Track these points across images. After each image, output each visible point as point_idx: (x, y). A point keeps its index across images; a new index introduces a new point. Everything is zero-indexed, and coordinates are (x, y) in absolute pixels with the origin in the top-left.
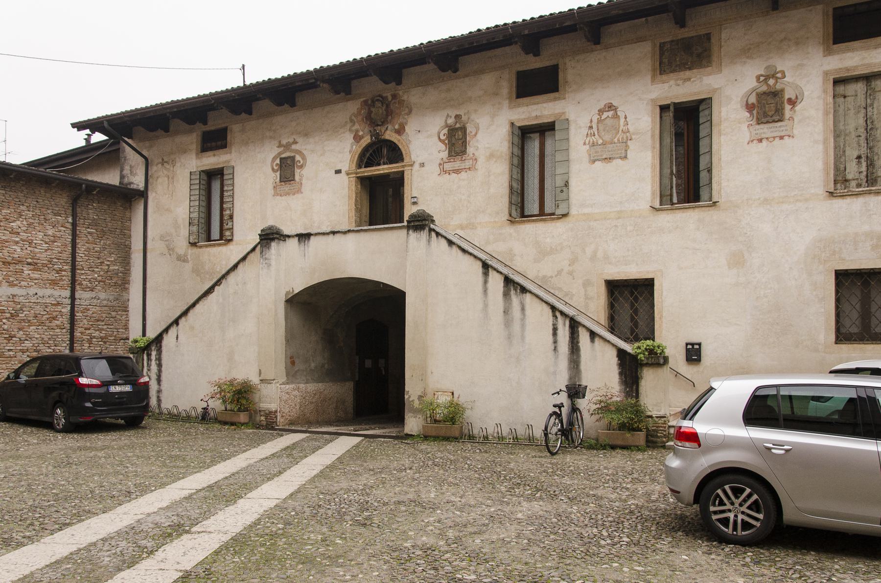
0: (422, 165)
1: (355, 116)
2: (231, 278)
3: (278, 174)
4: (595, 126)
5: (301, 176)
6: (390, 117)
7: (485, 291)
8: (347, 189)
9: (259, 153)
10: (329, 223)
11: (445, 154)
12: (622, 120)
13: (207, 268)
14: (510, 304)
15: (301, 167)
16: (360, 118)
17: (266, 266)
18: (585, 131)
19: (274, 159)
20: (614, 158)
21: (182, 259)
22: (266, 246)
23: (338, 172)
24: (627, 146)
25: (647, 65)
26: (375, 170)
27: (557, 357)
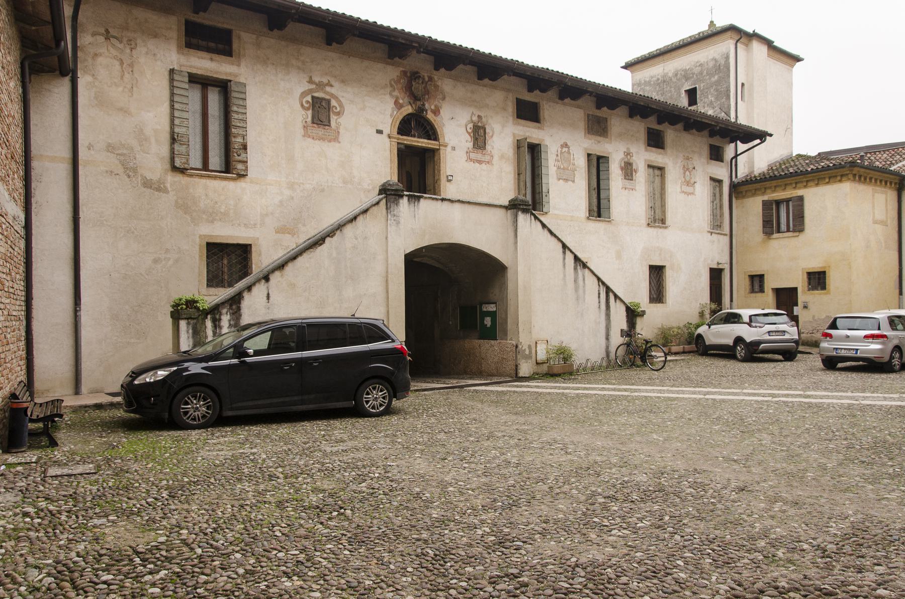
0: (454, 148)
1: (395, 82)
2: (348, 230)
3: (310, 113)
4: (559, 155)
5: (338, 124)
6: (427, 96)
7: (564, 265)
8: (388, 152)
9: (281, 80)
10: (370, 182)
11: (470, 145)
12: (572, 156)
13: (202, 205)
14: (578, 275)
15: (338, 114)
16: (400, 86)
17: (395, 222)
18: (555, 157)
19: (303, 94)
20: (569, 180)
21: (158, 187)
22: (394, 202)
23: (380, 132)
24: (574, 174)
25: (582, 124)
26: (415, 141)
27: (600, 312)
